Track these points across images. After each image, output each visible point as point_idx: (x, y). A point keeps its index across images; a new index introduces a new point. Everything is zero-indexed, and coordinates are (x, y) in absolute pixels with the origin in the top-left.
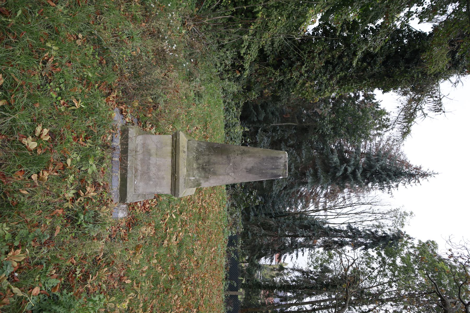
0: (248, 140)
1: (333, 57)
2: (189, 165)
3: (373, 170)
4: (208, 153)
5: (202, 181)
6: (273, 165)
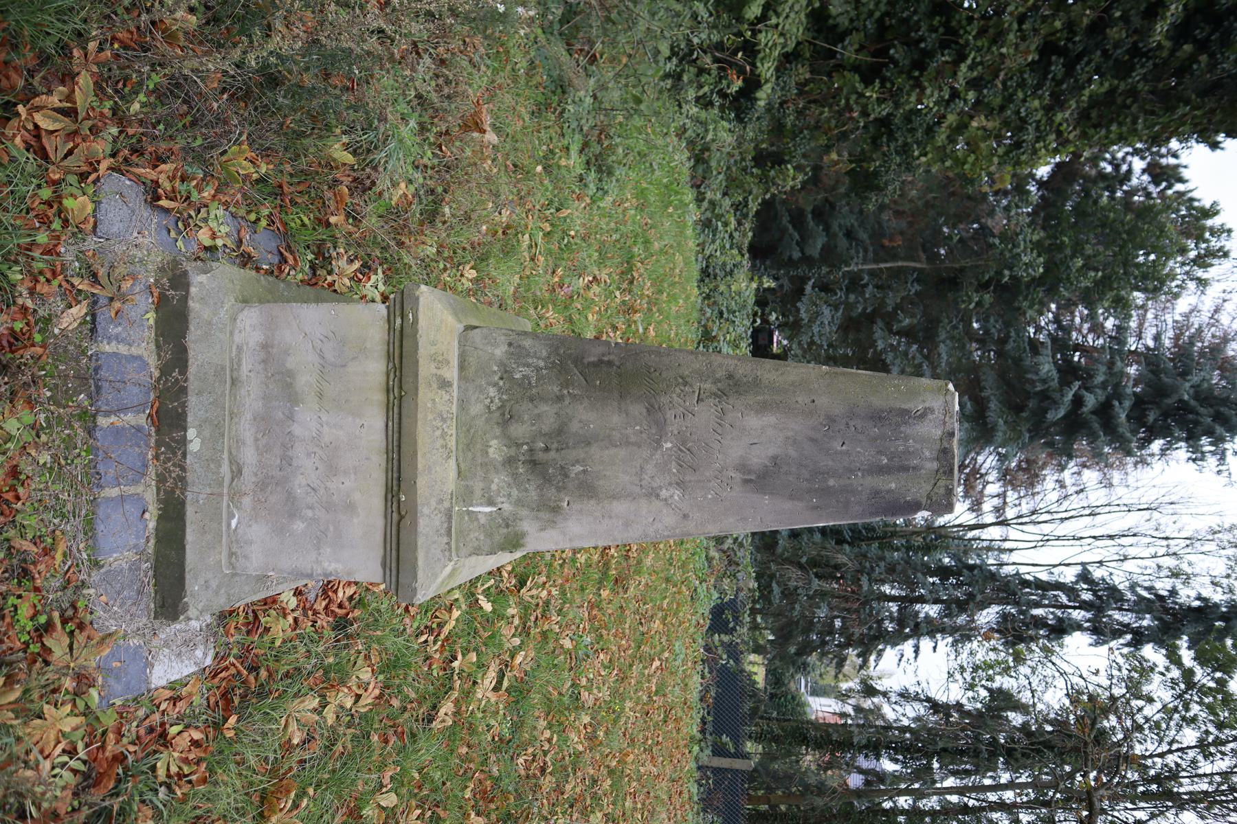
0: (773, 317)
1: (1070, 26)
2: (468, 447)
3: (1169, 401)
4: (556, 389)
5: (528, 526)
6: (880, 453)
